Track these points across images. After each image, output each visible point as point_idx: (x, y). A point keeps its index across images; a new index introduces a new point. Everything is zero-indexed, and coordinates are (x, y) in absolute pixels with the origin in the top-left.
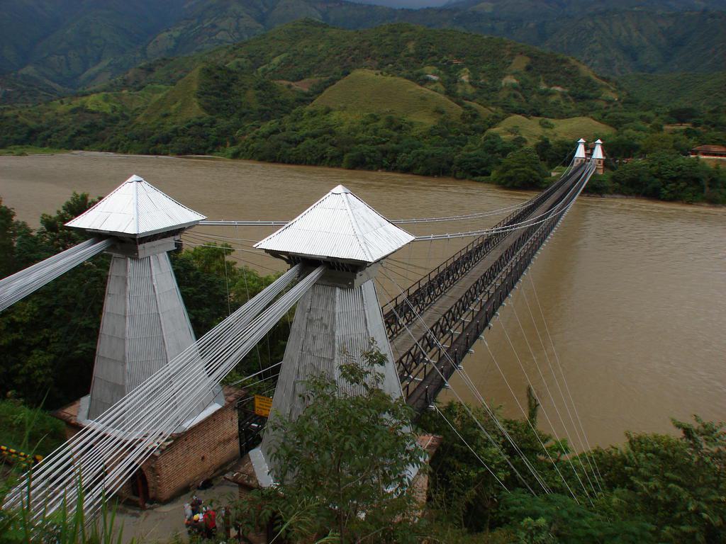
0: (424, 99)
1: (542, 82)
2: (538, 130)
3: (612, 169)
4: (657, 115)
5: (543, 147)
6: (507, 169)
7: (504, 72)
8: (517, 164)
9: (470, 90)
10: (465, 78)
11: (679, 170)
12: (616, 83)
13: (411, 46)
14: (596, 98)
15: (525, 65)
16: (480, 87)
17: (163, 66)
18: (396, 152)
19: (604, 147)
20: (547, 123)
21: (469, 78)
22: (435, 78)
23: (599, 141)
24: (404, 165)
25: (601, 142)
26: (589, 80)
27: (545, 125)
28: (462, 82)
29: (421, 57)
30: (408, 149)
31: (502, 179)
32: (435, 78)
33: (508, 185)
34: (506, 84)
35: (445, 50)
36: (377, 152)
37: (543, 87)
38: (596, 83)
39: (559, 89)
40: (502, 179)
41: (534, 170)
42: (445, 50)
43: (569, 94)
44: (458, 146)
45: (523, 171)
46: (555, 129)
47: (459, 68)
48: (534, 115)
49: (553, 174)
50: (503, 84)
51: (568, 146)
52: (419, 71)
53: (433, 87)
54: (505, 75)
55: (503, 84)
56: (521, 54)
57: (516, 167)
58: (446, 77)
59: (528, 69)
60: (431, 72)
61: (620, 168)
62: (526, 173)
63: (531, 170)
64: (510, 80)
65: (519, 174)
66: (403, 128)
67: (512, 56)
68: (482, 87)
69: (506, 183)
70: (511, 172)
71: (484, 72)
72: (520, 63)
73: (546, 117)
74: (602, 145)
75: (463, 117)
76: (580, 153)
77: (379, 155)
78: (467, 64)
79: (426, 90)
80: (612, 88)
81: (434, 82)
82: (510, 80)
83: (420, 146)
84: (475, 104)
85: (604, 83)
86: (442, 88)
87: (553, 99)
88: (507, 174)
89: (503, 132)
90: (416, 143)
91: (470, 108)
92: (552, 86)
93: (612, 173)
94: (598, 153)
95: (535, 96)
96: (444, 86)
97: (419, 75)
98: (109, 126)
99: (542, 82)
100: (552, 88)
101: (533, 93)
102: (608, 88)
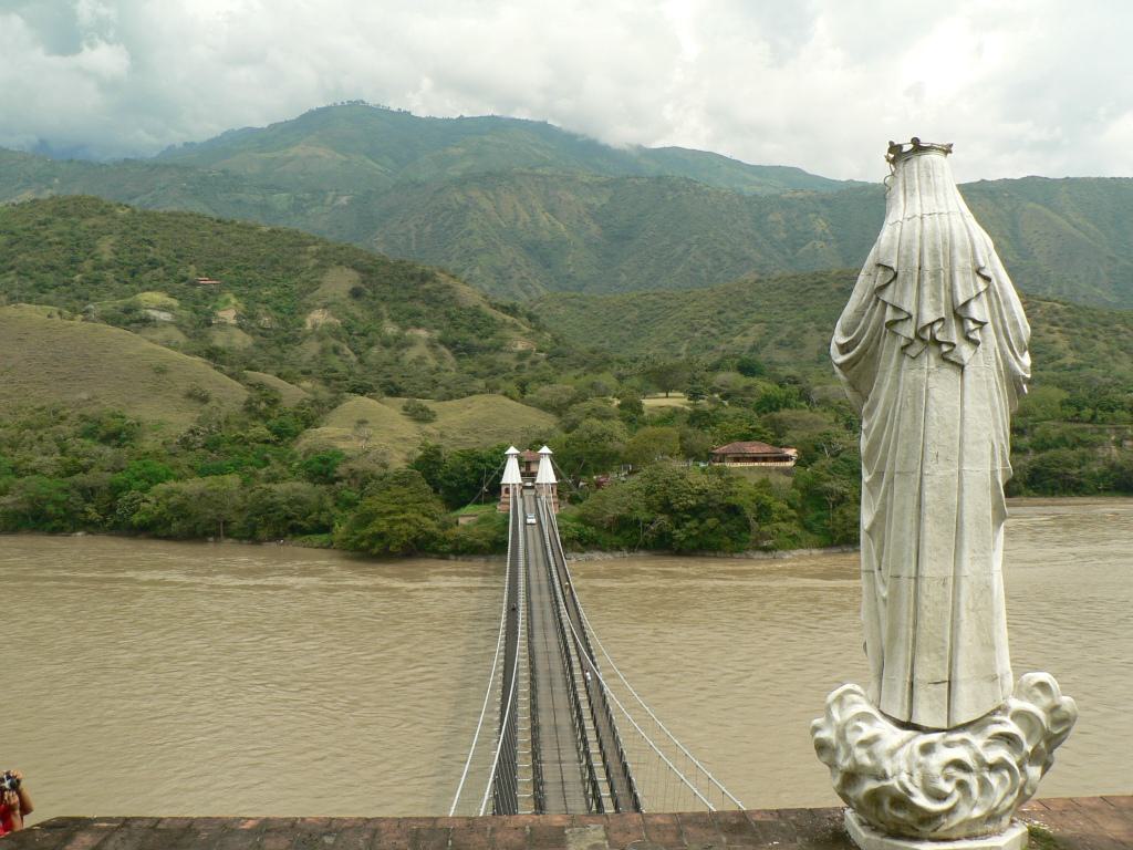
0: (161, 371)
1: (387, 322)
2: (409, 428)
3: (574, 500)
4: (621, 378)
5: (428, 463)
6: (366, 520)
7: (306, 300)
8: (392, 507)
9: (242, 340)
10: (228, 315)
11: (700, 493)
12: (531, 317)
13: (105, 249)
14: (498, 349)
15: (350, 287)
16: (262, 335)
17: (646, 448)
18: (116, 490)
19: (556, 460)
20: (424, 409)
21: (237, 317)
22: (164, 316)
23: (545, 450)
24: (136, 519)
25: (517, 452)
26: (476, 312)
27: (421, 416)
28: (223, 325)
29: (134, 273)
30: (143, 483)
31: (362, 540)
32: (164, 316)
33: (375, 551)
34: (315, 326)
35: (181, 257)
36: (73, 491)
37: (391, 329)
38: (492, 319)
39: (422, 333)
40: (362, 540)
41: (425, 515)
42: (181, 257)
43: (441, 341)
44: (251, 468)
45: (404, 520)
46: (440, 422)
47: (209, 294)
48: (390, 394)
49: (462, 521)
50: (309, 326)
51: (483, 461)
52: (128, 300)
53: (159, 335)
54: (310, 308)
55: (309, 326)
56: (340, 264)
57: (390, 513)
58: (186, 313)
59: (356, 294)
60: (152, 301)
61: (592, 500)
62: (410, 523)
63: (420, 517)
64: (318, 318)
65: (396, 528)
66: (124, 435)
67: (322, 267)
68: (264, 332)
69: (372, 546)
70: (381, 525)
71: (266, 302)
72: (339, 282)
73: (414, 395)
74: (551, 456)
75: (249, 407)
76: (512, 475)
77: (75, 498)
78: (229, 285)
79: (140, 345)
80: (524, 328)
81: (165, 324)
82: (318, 318)
83: (168, 476)
84: (270, 376)
85: (509, 319)
86: (180, 337)
87: (411, 354)
88: (370, 530)
89: (334, 433)
90: (158, 467)
91: (260, 386)
92: (406, 328)
93: (576, 510)
94: (546, 473)
95: (375, 350)
96: (185, 332)
97: (128, 311)
98: (893, 464)
99: (387, 322)
100: (408, 333)
101: (370, 345)
102: (515, 326)
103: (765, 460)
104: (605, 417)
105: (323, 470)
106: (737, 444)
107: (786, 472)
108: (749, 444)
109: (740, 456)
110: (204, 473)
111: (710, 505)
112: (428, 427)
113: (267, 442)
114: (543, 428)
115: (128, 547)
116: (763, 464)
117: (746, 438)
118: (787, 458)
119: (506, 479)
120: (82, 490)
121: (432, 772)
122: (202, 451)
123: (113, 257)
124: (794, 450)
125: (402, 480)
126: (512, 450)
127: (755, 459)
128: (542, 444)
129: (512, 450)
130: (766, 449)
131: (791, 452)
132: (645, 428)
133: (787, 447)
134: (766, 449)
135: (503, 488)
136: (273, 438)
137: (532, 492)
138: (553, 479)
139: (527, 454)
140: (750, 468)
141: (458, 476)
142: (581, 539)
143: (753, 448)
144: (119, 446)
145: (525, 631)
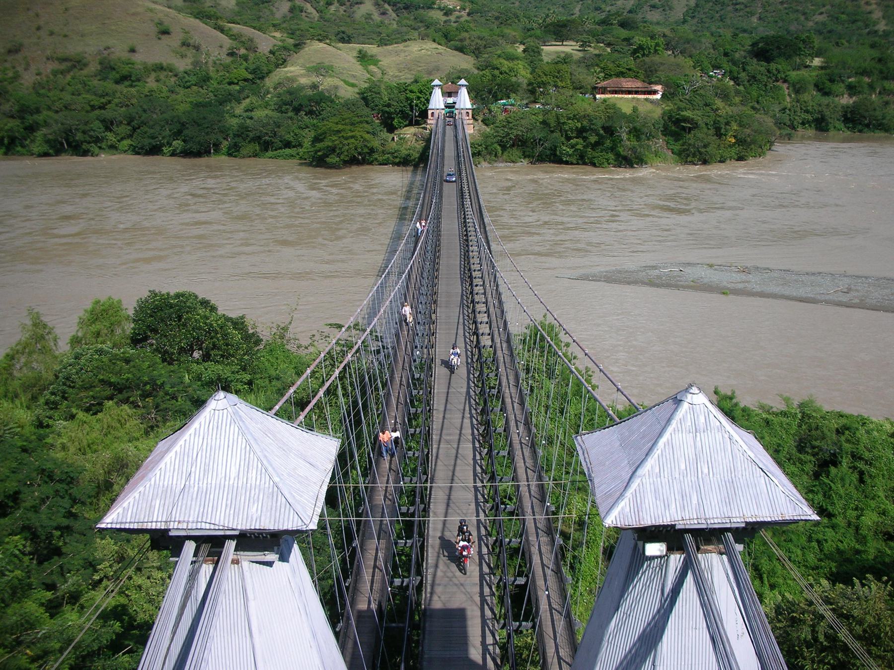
23: (463, 82)
45: (352, 137)
76: (437, 101)
94: (464, 100)
103: (637, 93)
104: (511, 58)
106: (614, 79)
107: (652, 102)
109: (617, 89)
111: (592, 127)
113: (246, 80)
116: (635, 96)
118: (655, 92)
120: (103, 121)
122: (195, 88)
124: (660, 86)
125: (349, 105)
126: (437, 82)
127: (629, 92)
129: (437, 82)
130: (638, 84)
131: (658, 88)
132: (703, 167)
133: (656, 83)
134: (638, 84)
135: (430, 112)
136: (250, 77)
140: (621, 98)
141: (395, 104)
143: (627, 83)
144: (131, 86)
145: (472, 261)
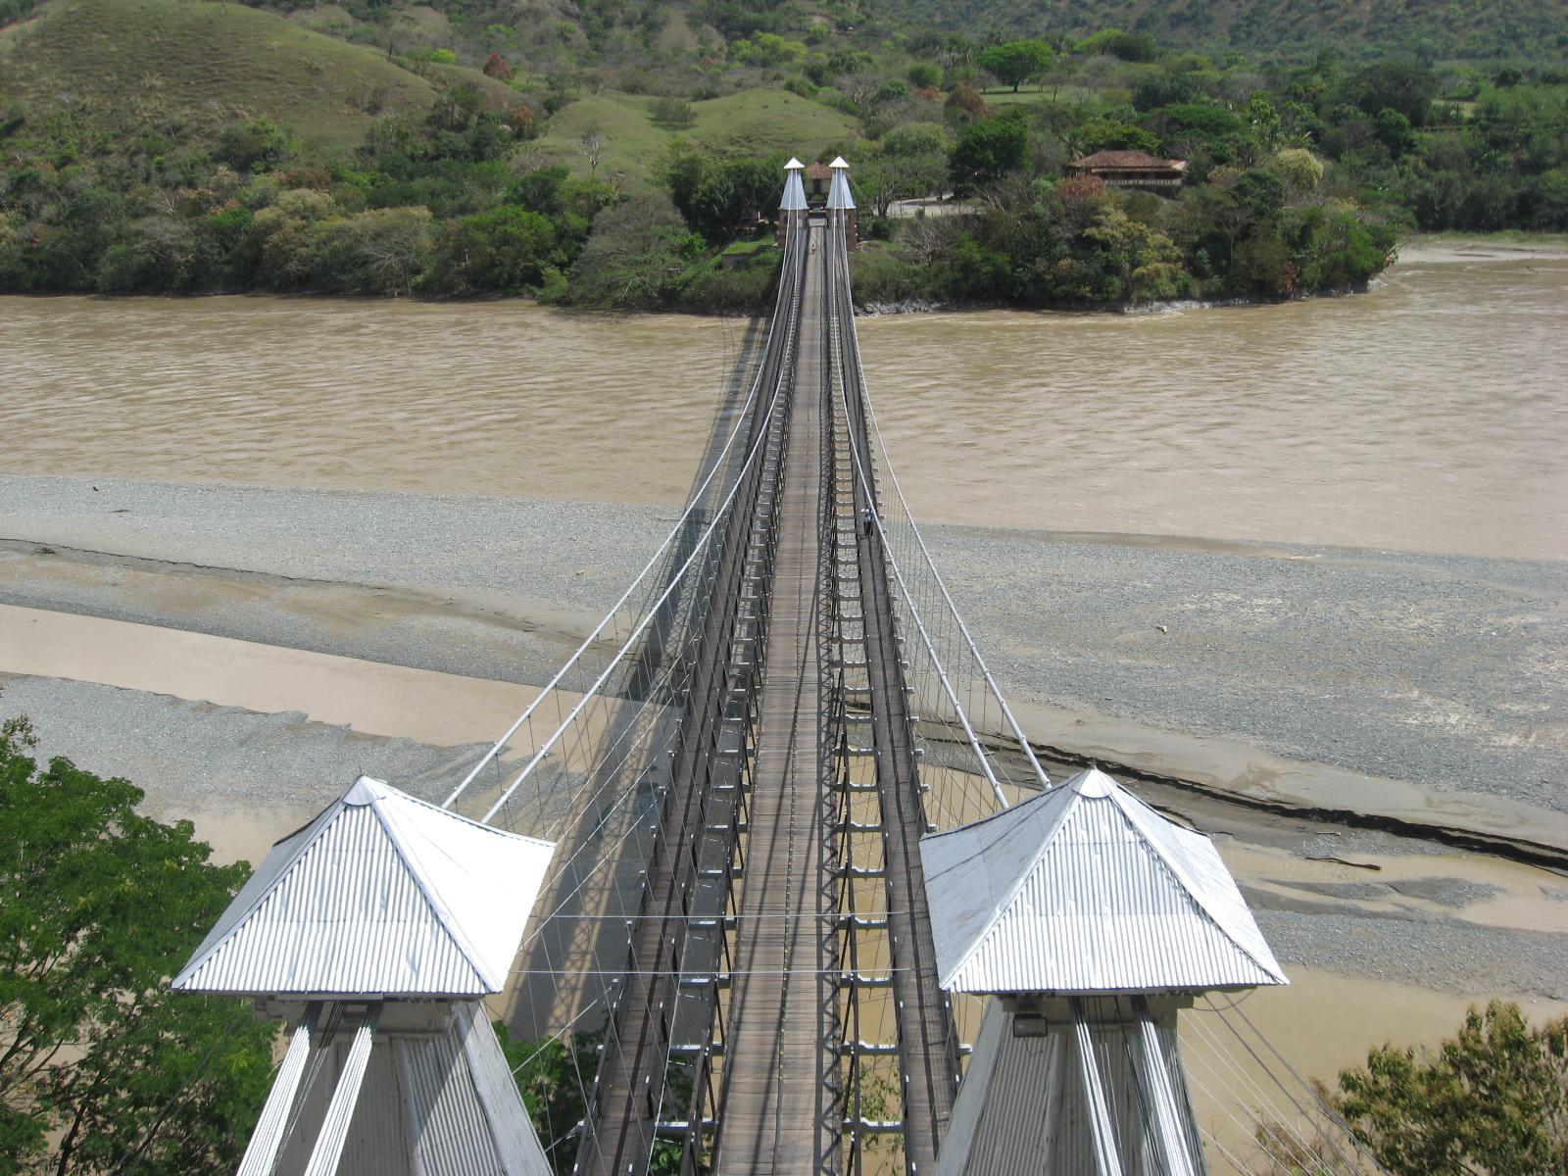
23: (839, 162)
76: (794, 197)
105: (540, 194)
106: (1104, 153)
108: (1122, 154)
110: (377, 202)
112: (683, 136)
114: (843, 132)
115: (1348, 313)
117: (1116, 146)
119: (787, 204)
121: (1372, 438)
123: (1177, 138)
128: (832, 154)
129: (794, 164)
130: (1146, 161)
131: (1179, 166)
137: (822, 222)
138: (850, 204)
139: (815, 170)
142: (865, 294)
